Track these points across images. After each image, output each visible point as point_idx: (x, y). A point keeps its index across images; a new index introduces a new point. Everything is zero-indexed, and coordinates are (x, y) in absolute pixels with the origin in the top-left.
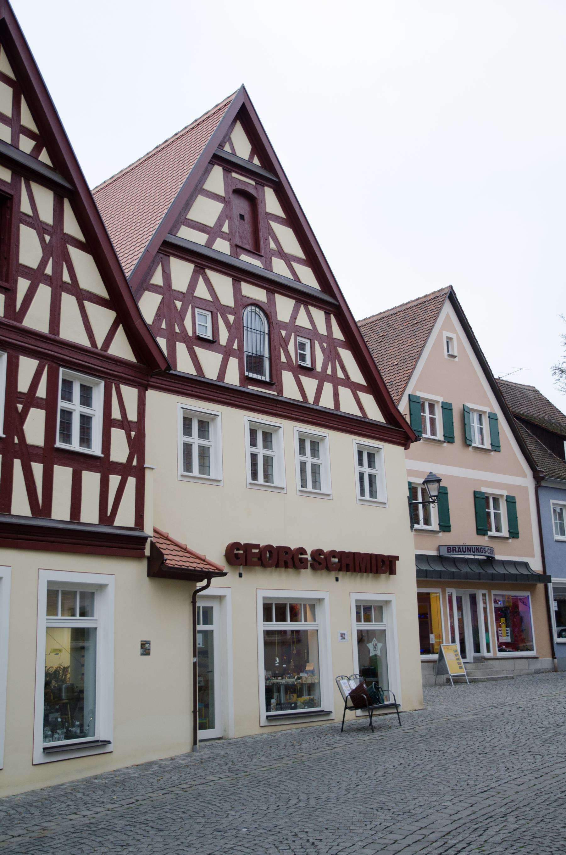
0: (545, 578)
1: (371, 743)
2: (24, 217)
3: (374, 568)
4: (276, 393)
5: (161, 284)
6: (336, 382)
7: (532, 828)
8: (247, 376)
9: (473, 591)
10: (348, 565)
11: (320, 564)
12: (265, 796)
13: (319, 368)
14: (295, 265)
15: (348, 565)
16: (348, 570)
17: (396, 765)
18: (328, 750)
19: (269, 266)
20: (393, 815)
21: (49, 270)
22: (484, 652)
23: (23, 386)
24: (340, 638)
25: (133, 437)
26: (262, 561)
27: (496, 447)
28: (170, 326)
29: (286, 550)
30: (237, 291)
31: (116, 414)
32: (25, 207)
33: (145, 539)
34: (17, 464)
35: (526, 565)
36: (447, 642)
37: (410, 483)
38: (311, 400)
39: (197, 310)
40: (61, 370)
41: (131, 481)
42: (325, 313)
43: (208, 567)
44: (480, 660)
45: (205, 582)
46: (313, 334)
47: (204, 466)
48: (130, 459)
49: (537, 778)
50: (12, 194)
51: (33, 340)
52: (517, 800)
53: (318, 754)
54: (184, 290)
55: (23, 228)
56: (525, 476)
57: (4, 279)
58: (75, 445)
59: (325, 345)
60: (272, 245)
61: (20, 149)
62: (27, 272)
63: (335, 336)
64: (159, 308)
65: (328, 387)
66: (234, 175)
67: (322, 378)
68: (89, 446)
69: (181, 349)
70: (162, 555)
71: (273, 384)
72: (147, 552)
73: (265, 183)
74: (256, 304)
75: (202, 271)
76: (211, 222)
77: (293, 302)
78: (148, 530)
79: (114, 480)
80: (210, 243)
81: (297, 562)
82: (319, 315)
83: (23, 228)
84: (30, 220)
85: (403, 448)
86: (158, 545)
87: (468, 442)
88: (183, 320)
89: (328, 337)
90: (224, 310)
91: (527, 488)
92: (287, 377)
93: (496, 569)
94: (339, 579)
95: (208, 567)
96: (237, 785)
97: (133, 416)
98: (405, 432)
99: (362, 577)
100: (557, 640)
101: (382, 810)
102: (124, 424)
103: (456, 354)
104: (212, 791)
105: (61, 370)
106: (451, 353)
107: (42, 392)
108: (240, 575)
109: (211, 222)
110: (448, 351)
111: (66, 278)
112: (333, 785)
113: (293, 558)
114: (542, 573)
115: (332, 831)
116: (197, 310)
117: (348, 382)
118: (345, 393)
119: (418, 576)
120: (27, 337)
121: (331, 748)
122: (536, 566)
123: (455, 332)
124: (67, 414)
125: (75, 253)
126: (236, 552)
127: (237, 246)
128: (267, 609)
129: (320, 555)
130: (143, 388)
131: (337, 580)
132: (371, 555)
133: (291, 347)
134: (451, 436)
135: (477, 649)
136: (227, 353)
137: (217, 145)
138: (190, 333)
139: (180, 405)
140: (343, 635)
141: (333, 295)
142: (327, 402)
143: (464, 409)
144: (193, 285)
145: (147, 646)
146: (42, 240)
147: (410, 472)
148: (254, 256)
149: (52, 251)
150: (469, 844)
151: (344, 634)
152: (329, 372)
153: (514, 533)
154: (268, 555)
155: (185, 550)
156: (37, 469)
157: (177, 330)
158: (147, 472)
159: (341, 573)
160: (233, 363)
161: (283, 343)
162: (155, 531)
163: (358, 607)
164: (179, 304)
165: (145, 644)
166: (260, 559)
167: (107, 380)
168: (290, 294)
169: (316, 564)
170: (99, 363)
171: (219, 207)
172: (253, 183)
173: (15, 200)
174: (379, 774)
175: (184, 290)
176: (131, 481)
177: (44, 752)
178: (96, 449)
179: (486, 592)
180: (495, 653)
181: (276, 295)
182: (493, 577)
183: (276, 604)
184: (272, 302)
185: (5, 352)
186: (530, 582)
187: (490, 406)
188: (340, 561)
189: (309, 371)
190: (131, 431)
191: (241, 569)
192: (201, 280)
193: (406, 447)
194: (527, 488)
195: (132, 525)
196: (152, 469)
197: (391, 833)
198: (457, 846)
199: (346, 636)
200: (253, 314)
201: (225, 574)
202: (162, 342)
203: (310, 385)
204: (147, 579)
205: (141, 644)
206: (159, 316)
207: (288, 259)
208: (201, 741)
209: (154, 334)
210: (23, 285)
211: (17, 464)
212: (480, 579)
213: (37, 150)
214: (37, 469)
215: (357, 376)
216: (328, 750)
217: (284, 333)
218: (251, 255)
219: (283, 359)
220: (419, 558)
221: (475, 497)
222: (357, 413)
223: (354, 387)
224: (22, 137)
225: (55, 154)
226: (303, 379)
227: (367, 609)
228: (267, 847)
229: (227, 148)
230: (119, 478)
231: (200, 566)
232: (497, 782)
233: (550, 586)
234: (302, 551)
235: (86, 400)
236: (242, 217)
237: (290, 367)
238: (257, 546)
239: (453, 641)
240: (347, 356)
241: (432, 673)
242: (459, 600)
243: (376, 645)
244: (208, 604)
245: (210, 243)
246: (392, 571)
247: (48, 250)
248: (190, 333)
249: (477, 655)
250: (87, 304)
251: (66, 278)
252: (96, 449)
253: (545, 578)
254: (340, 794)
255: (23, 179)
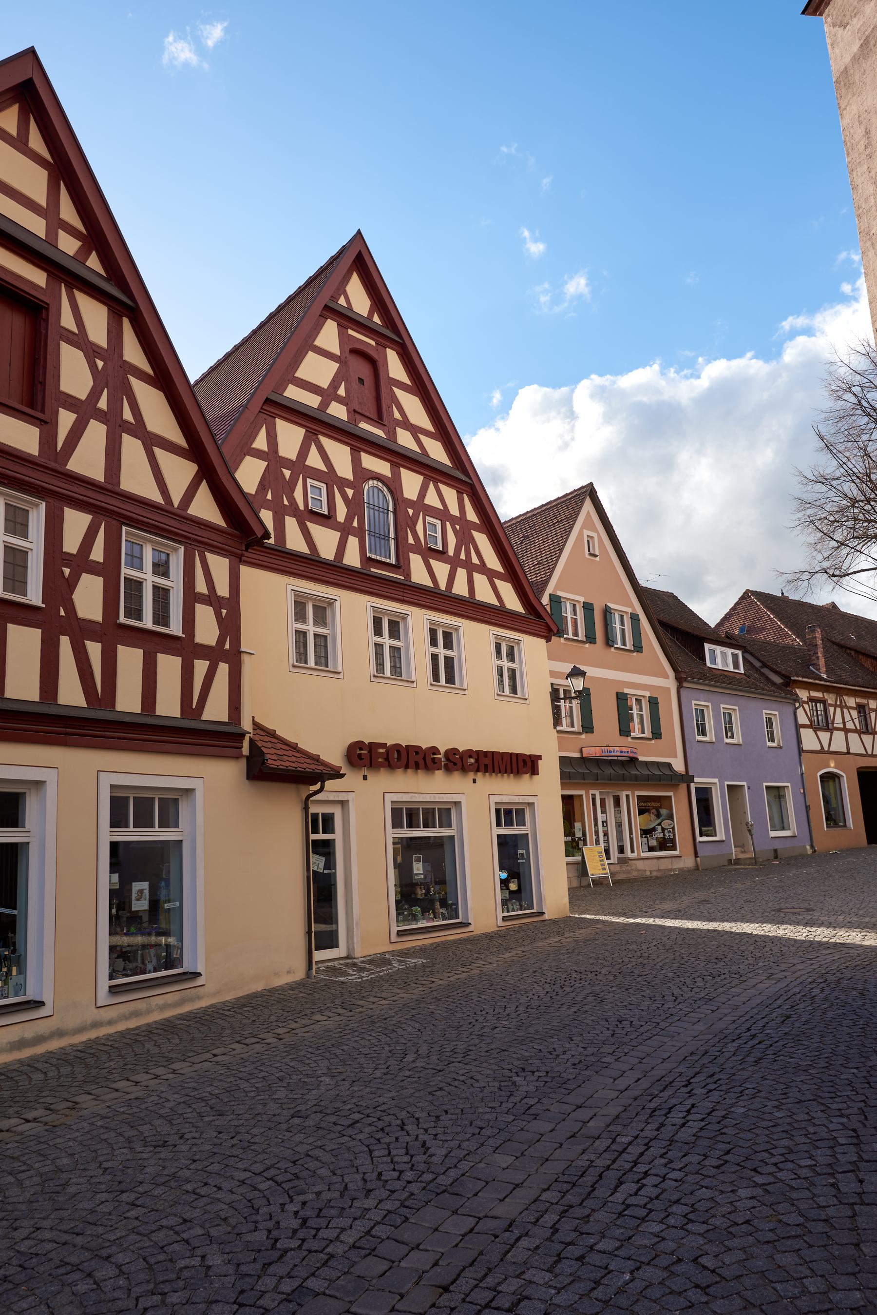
0: (687, 778)
1: (513, 961)
2: (65, 333)
3: (515, 770)
4: (403, 578)
5: (265, 449)
6: (471, 569)
7: (732, 1109)
8: (369, 557)
9: (616, 792)
10: (486, 766)
11: (455, 764)
12: (375, 1049)
13: (451, 552)
14: (424, 439)
15: (486, 766)
16: (486, 770)
17: (541, 995)
18: (464, 972)
19: (393, 436)
20: (537, 1084)
21: (103, 404)
22: (629, 854)
23: (71, 544)
25: (224, 616)
26: (389, 762)
27: (638, 647)
28: (277, 497)
29: (417, 750)
30: (356, 463)
31: (201, 587)
32: (67, 320)
33: (242, 736)
34: (65, 642)
35: (669, 765)
36: (592, 844)
37: (552, 684)
38: (443, 586)
39: (309, 480)
40: (124, 528)
41: (223, 669)
42: (457, 491)
43: (321, 768)
44: (623, 861)
45: (318, 786)
46: (443, 515)
47: (323, 658)
48: (221, 640)
49: (713, 1011)
50: (48, 302)
51: (82, 489)
52: (698, 1052)
53: (451, 979)
54: (293, 457)
55: (65, 347)
56: (667, 677)
57: (40, 408)
58: (148, 622)
59: (458, 527)
60: (397, 415)
61: (60, 247)
62: (71, 403)
63: (469, 518)
64: (263, 474)
65: (462, 573)
66: (350, 332)
67: (455, 563)
68: (167, 624)
69: (291, 523)
70: (263, 753)
71: (400, 568)
72: (245, 750)
73: (386, 343)
74: (378, 477)
75: (314, 437)
76: (324, 383)
77: (422, 478)
78: (247, 725)
79: (201, 667)
80: (324, 405)
81: (429, 761)
82: (450, 494)
83: (65, 347)
84: (75, 338)
85: (544, 641)
86: (260, 744)
87: (610, 643)
88: (293, 491)
89: (460, 518)
90: (343, 483)
91: (669, 689)
92: (416, 561)
93: (640, 770)
95: (321, 768)
96: (345, 1030)
97: (223, 590)
98: (547, 623)
100: (699, 839)
101: (524, 1074)
102: (212, 599)
103: (597, 553)
104: (312, 1040)
105: (124, 528)
106: (592, 552)
107: (97, 554)
109: (324, 383)
110: (589, 551)
111: (128, 415)
112: (464, 1028)
113: (424, 759)
114: (684, 773)
115: (454, 1117)
116: (309, 480)
117: (483, 568)
118: (480, 580)
119: (562, 778)
120: (74, 484)
121: (467, 970)
122: (678, 766)
123: (597, 531)
124: (135, 586)
125: (139, 387)
126: (358, 752)
127: (355, 411)
128: (396, 813)
129: (455, 754)
130: (237, 559)
132: (511, 755)
133: (419, 528)
134: (593, 637)
135: (621, 850)
136: (345, 530)
137: (329, 297)
138: (301, 507)
139: (290, 587)
141: (465, 472)
142: (460, 588)
143: (606, 610)
144: (304, 452)
146: (93, 366)
147: (553, 674)
148: (376, 424)
149: (107, 380)
150: (647, 1146)
152: (463, 556)
153: (657, 734)
154: (396, 756)
155: (295, 749)
156: (94, 650)
157: (286, 502)
158: (245, 658)
159: (479, 774)
160: (353, 542)
161: (410, 523)
162: (256, 725)
163: (498, 811)
164: (287, 473)
166: (387, 759)
167: (188, 545)
169: (451, 764)
170: (177, 525)
171: (333, 367)
172: (373, 343)
173: (52, 310)
174: (521, 1009)
175: (293, 457)
176: (223, 669)
177: (110, 991)
178: (176, 628)
179: (629, 793)
180: (639, 854)
181: (402, 469)
182: (636, 778)
184: (397, 476)
185: (42, 499)
186: (673, 782)
187: (632, 606)
188: (477, 761)
189: (441, 555)
190: (221, 608)
191: (365, 772)
192: (313, 448)
193: (548, 640)
194: (669, 689)
195: (225, 719)
196: (251, 654)
197: (535, 1119)
198: (630, 1149)
200: (376, 490)
201: (343, 776)
202: (267, 517)
203: (441, 570)
204: (247, 782)
206: (263, 486)
207: (415, 431)
208: (317, 962)
209: (255, 506)
210: (66, 419)
211: (65, 642)
212: (624, 780)
213: (85, 252)
214: (94, 650)
215: (493, 562)
216: (464, 972)
217: (411, 511)
219: (411, 540)
220: (562, 759)
221: (617, 698)
222: (494, 601)
223: (491, 575)
224: (61, 233)
225: (107, 259)
226: (434, 563)
227: (508, 812)
228: (356, 1150)
229: (342, 301)
230: (207, 663)
231: (310, 767)
232: (668, 1020)
233: (693, 786)
234: (434, 750)
235: (161, 569)
236: (361, 381)
237: (418, 548)
238: (383, 745)
239: (598, 843)
240: (482, 540)
241: (576, 875)
242: (603, 801)
244: (327, 810)
245: (324, 405)
246: (534, 771)
247: (100, 380)
248: (301, 507)
249: (622, 855)
250: (157, 451)
251: (128, 415)
252: (176, 628)
253: (687, 778)
254: (470, 1043)
255: (63, 284)
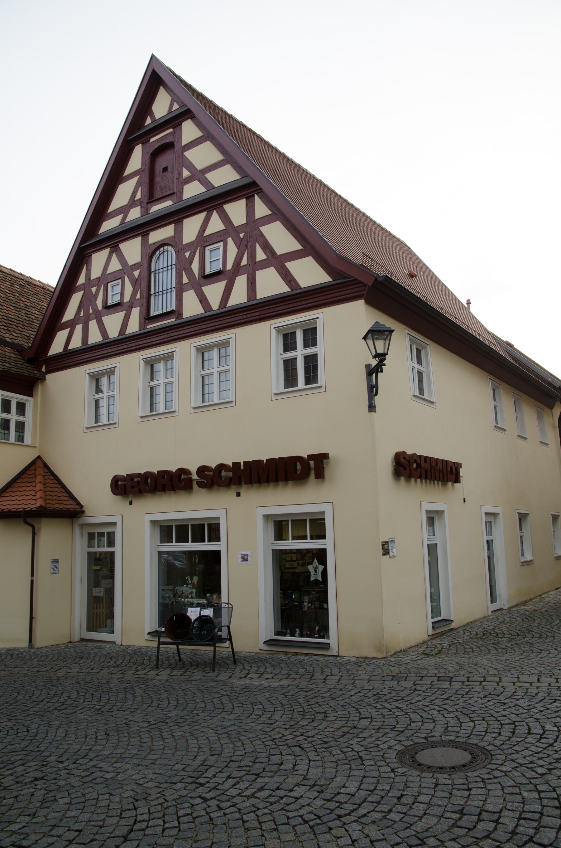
24: (241, 559)
94: (241, 494)
99: (286, 485)
108: (131, 503)
131: (238, 495)
140: (246, 557)
145: (386, 546)
151: (247, 555)
165: (384, 545)
168: (197, 210)
183: (176, 525)
199: (249, 557)
205: (382, 545)
218: (162, 200)
234: (182, 471)
243: (317, 567)
